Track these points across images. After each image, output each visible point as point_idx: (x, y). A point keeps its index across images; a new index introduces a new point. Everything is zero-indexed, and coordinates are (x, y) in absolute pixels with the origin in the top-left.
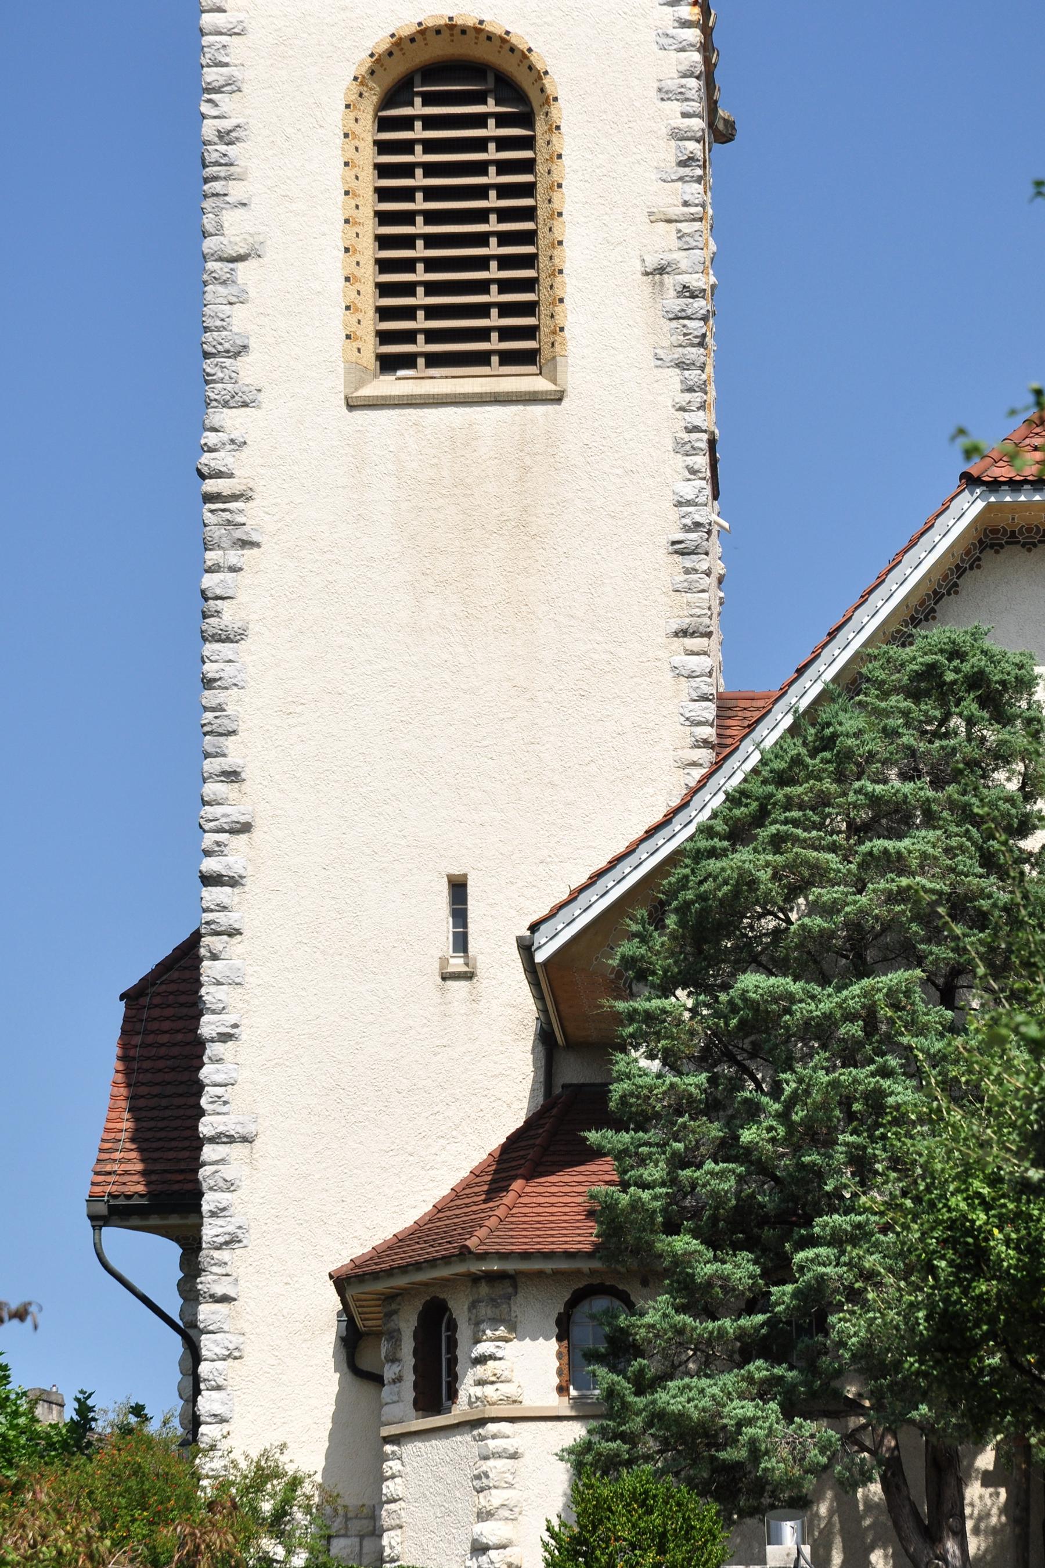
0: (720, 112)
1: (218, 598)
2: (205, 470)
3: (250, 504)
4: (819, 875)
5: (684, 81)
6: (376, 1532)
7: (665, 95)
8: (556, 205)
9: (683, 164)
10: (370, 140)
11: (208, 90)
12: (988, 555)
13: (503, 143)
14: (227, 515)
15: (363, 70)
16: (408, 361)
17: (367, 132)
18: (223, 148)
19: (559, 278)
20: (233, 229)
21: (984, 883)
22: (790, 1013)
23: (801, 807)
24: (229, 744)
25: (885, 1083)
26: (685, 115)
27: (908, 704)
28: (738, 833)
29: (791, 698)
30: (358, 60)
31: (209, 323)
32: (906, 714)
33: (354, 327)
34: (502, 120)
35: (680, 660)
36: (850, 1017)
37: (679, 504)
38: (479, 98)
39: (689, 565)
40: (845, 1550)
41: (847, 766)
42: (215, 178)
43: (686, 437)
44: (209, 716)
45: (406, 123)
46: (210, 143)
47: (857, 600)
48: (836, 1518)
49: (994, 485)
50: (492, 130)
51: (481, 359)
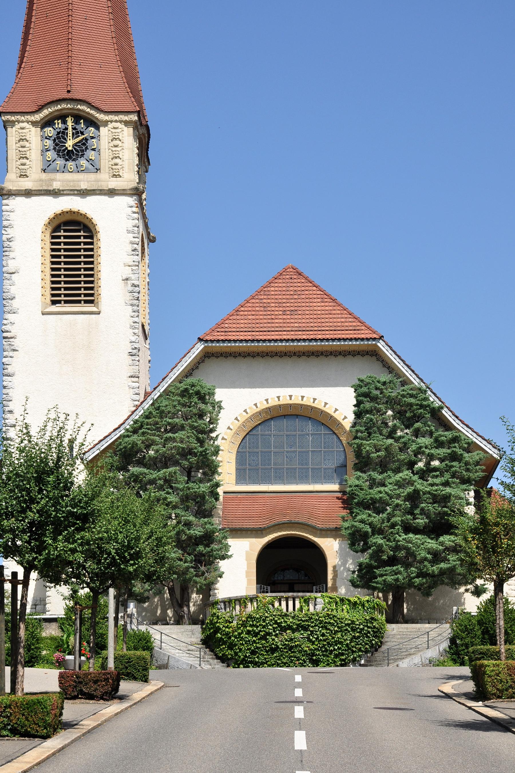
0: (151, 234)
1: (7, 365)
2: (3, 330)
3: (16, 340)
4: (153, 443)
5: (134, 228)
6: (45, 605)
7: (129, 232)
8: (99, 261)
9: (133, 251)
10: (49, 242)
11: (4, 227)
12: (207, 359)
13: (85, 243)
14: (9, 343)
15: (47, 223)
16: (59, 302)
17: (48, 239)
18: (8, 243)
19: (99, 281)
20: (11, 265)
21: (196, 445)
22: (145, 478)
23: (151, 425)
24: (10, 403)
25: (168, 496)
26: (134, 237)
27: (179, 398)
28: (135, 431)
29: (152, 396)
30: (46, 220)
31: (5, 290)
32: (179, 401)
33: (44, 292)
34: (85, 237)
35: (131, 384)
36: (160, 479)
37: (131, 342)
38: (79, 231)
39: (133, 359)
40: (161, 610)
41: (162, 414)
42: (6, 251)
43: (133, 324)
44: (5, 396)
45: (59, 237)
46: (5, 241)
47: (170, 370)
48: (159, 602)
49: (206, 341)
50: (82, 240)
51: (79, 302)
